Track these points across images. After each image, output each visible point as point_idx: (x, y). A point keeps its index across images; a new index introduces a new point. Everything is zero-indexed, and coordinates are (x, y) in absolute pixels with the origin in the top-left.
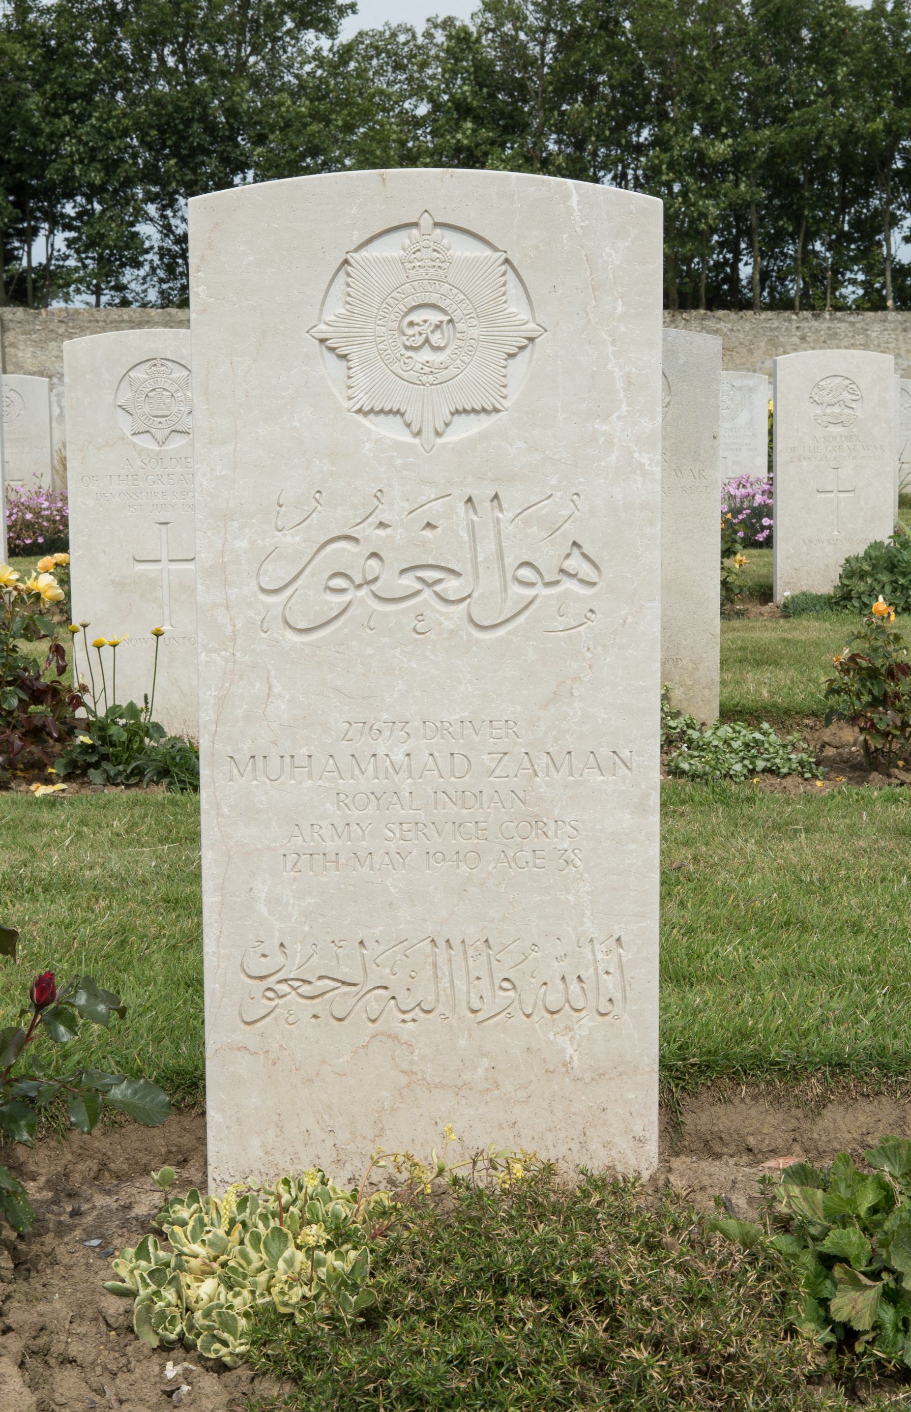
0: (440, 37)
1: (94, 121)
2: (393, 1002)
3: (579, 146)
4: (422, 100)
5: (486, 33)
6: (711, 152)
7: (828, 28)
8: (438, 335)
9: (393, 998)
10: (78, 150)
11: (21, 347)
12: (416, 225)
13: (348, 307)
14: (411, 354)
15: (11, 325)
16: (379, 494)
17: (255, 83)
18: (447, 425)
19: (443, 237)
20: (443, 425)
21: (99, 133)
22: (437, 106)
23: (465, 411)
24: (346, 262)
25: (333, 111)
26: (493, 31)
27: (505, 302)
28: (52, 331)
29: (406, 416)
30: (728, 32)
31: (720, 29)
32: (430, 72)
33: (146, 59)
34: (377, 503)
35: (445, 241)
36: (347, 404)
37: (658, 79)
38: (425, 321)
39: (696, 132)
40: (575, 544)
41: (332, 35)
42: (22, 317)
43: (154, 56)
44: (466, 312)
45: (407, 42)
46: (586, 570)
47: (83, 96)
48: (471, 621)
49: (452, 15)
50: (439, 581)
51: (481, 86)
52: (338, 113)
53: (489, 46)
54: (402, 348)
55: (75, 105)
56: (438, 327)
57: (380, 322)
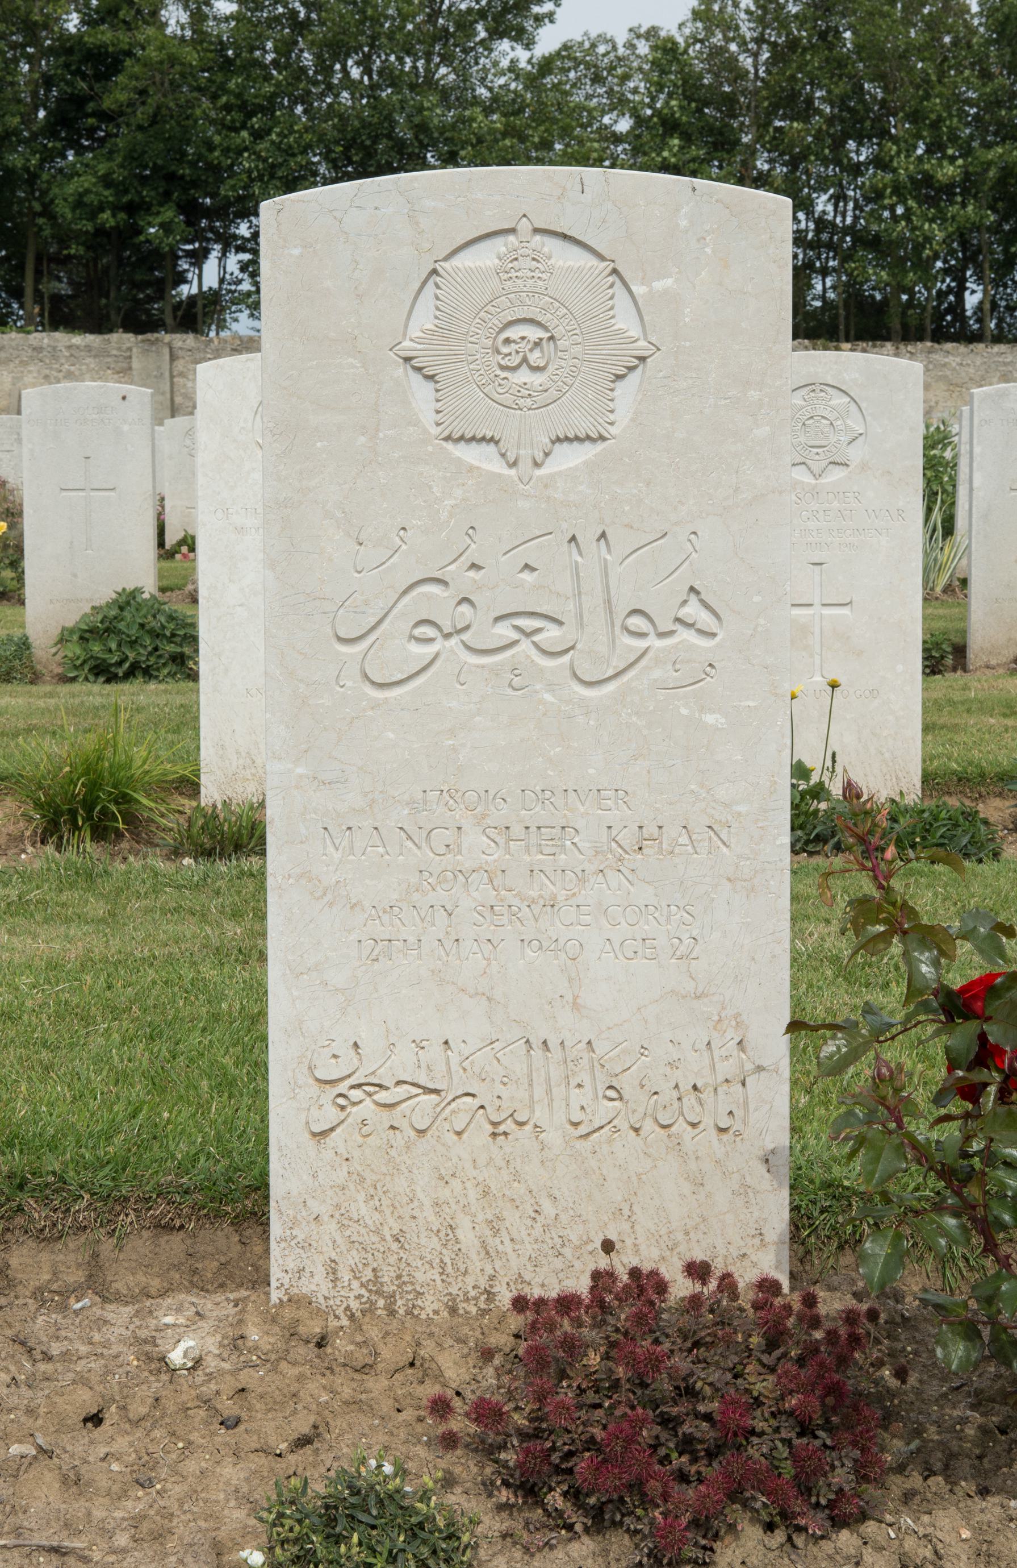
0: (643, 48)
1: (274, 137)
2: (481, 1111)
3: (794, 164)
4: (624, 115)
5: (694, 44)
6: (939, 176)
8: (537, 353)
9: (482, 1107)
10: (257, 166)
12: (512, 231)
14: (504, 374)
15: (180, 353)
16: (471, 531)
17: (444, 94)
18: (547, 454)
19: (543, 245)
20: (541, 454)
21: (279, 149)
22: (639, 121)
23: (567, 439)
24: (434, 272)
25: (529, 126)
26: (701, 41)
27: (613, 317)
29: (501, 444)
30: (955, 43)
31: (947, 39)
32: (632, 85)
33: (329, 71)
34: (469, 541)
35: (546, 250)
36: (435, 431)
37: (880, 94)
38: (523, 338)
39: (920, 152)
40: (692, 589)
41: (528, 46)
42: (193, 344)
43: (338, 67)
44: (568, 328)
45: (608, 53)
46: (704, 618)
48: (575, 675)
49: (656, 24)
50: (539, 630)
51: (690, 99)
52: (535, 129)
53: (696, 58)
55: (255, 119)
56: (537, 344)
57: (472, 339)
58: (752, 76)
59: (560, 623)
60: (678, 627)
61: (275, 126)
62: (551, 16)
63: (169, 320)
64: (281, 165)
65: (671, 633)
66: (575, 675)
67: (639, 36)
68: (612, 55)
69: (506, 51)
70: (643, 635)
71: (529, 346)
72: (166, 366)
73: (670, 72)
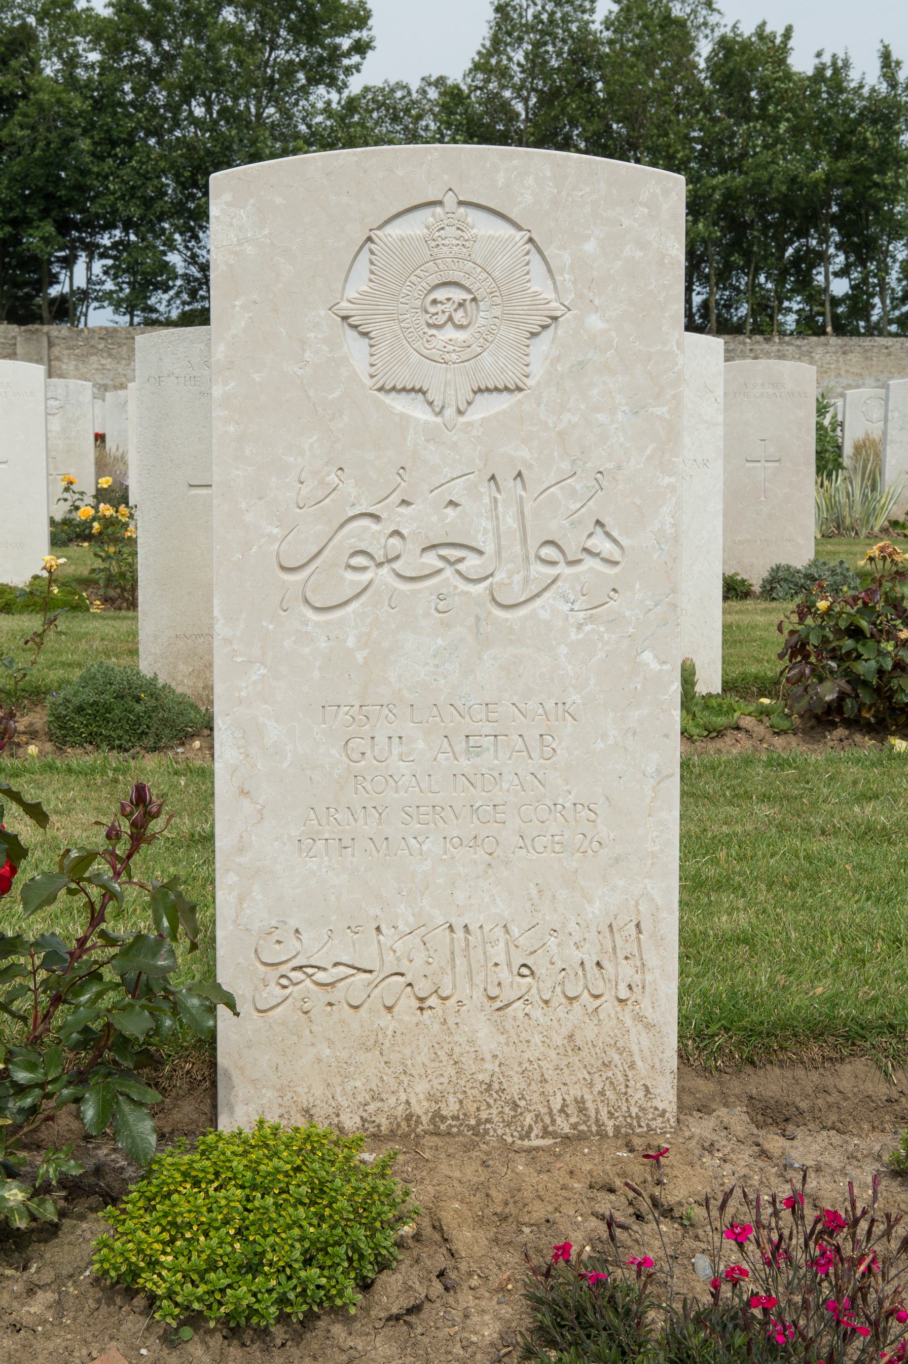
0: (433, 94)
1: (134, 163)
2: (409, 988)
5: (475, 90)
7: (772, 90)
8: (460, 313)
9: (410, 985)
10: (120, 188)
11: (65, 361)
12: (439, 203)
13: (371, 284)
15: (57, 341)
16: (401, 471)
18: (469, 403)
21: (138, 173)
23: (488, 390)
26: (481, 89)
28: (93, 346)
29: (428, 395)
32: (424, 123)
38: (449, 299)
40: (598, 523)
45: (403, 98)
47: (124, 141)
48: (494, 599)
49: (444, 74)
54: (424, 326)
55: (118, 149)
56: (461, 305)
58: (523, 116)
59: (480, 553)
60: (584, 556)
61: (135, 155)
62: (357, 67)
63: (45, 314)
64: (140, 187)
65: (578, 562)
66: (494, 599)
67: (430, 84)
68: (407, 99)
69: (321, 94)
70: (553, 563)
71: (455, 306)
72: (45, 352)
73: (456, 113)
